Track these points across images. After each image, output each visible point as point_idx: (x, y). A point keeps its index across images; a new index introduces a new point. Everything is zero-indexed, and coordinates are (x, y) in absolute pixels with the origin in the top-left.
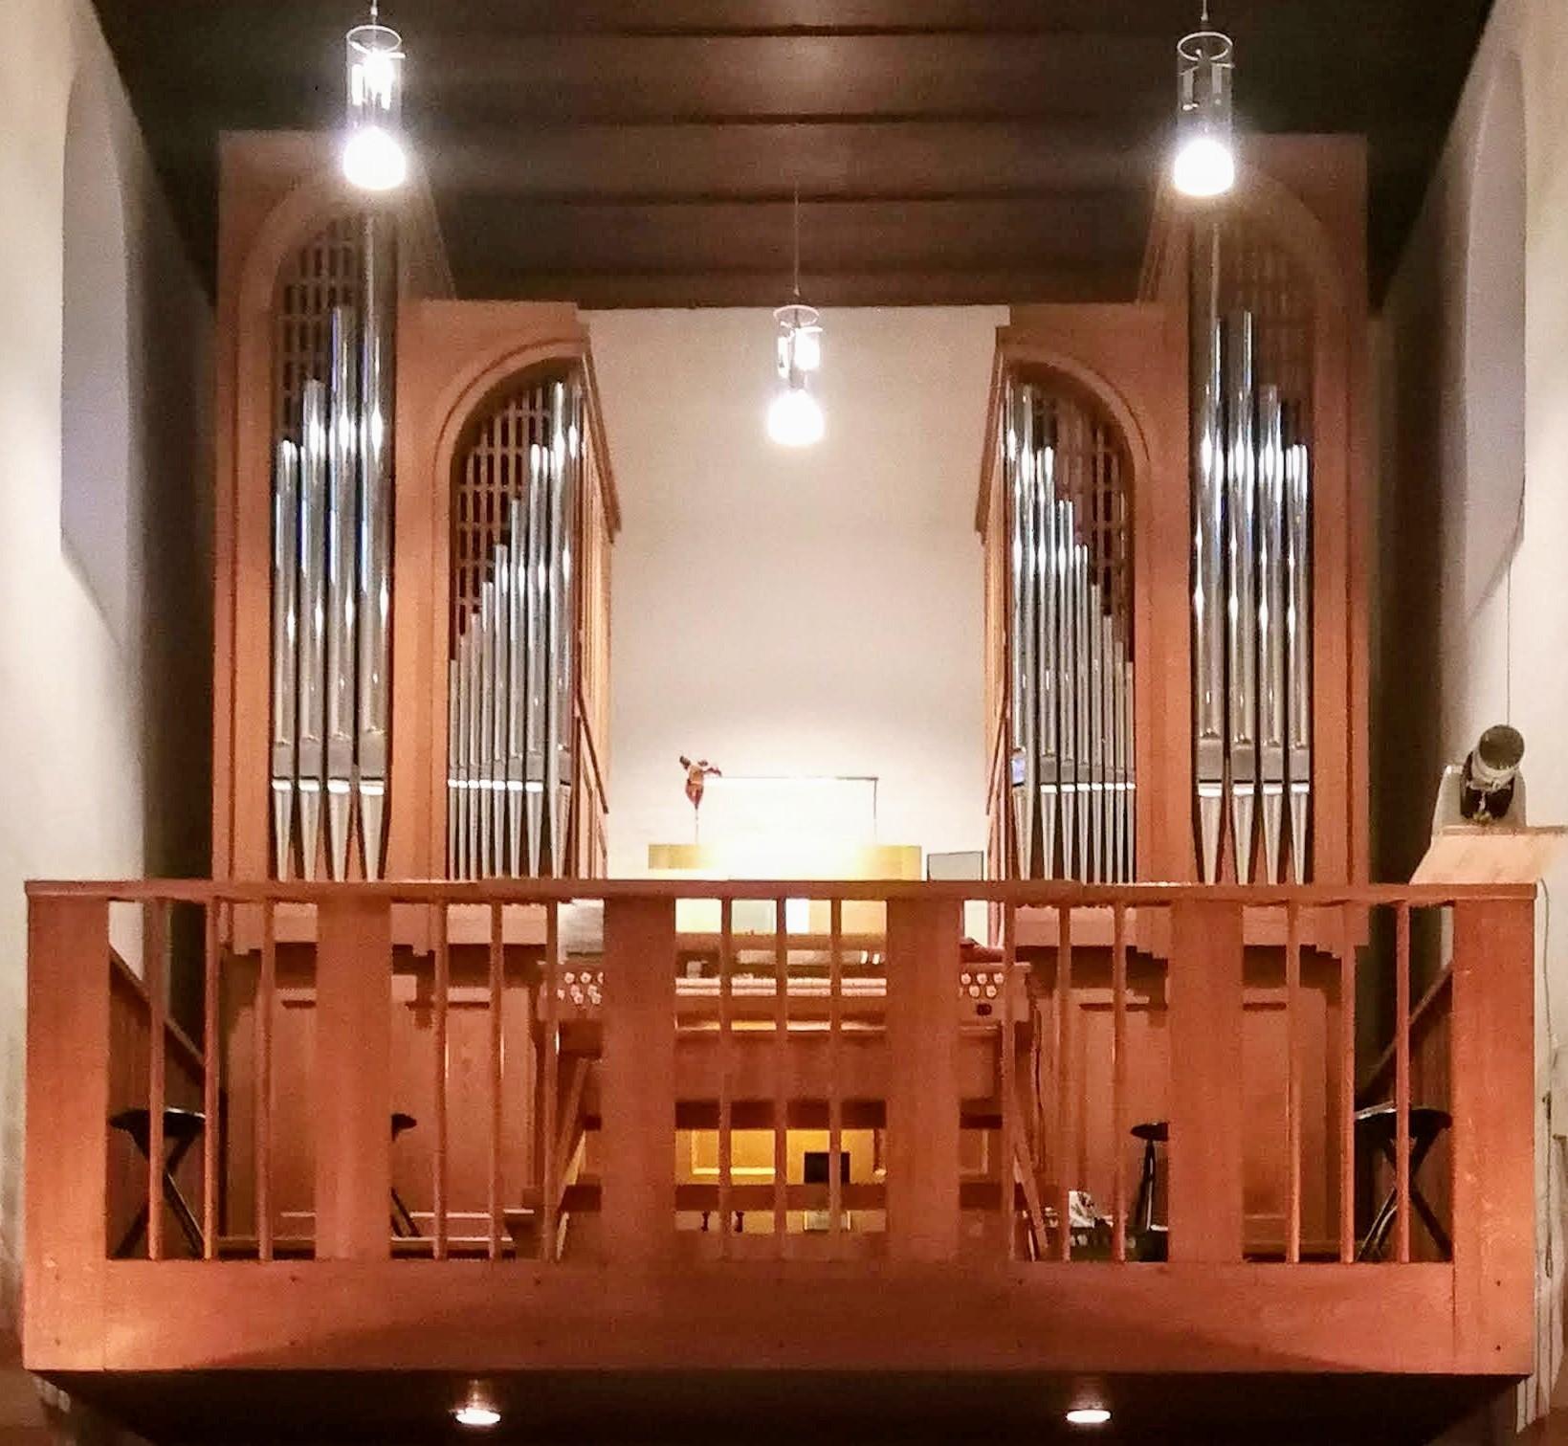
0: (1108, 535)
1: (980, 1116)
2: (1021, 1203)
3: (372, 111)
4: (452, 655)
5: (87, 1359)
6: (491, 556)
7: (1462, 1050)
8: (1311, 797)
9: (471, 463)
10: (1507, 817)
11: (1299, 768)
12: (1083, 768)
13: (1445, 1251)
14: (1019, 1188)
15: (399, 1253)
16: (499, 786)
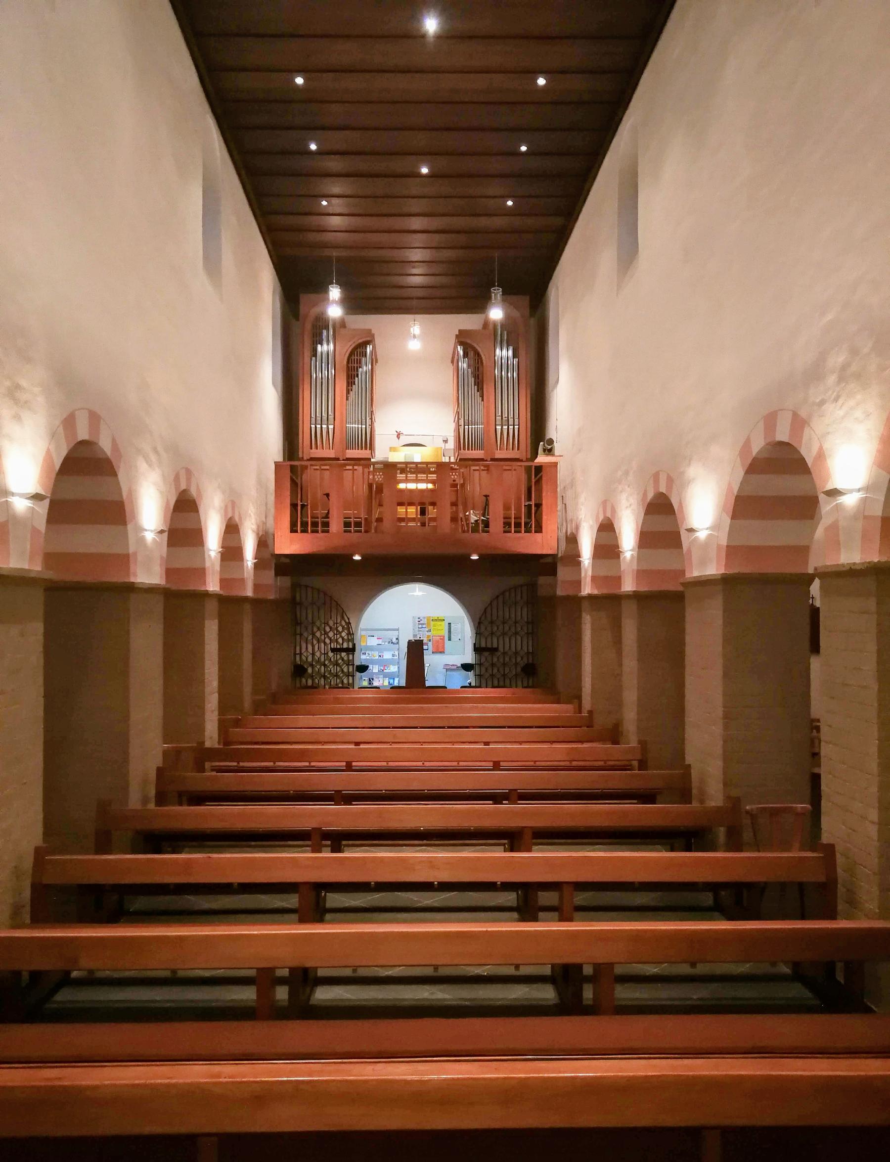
0: (478, 375)
1: (454, 504)
2: (462, 521)
3: (334, 302)
4: (347, 400)
5: (287, 551)
6: (354, 379)
7: (544, 486)
8: (519, 428)
9: (350, 360)
10: (551, 453)
11: (516, 423)
12: (473, 423)
13: (541, 531)
14: (461, 518)
15: (345, 531)
16: (356, 426)
